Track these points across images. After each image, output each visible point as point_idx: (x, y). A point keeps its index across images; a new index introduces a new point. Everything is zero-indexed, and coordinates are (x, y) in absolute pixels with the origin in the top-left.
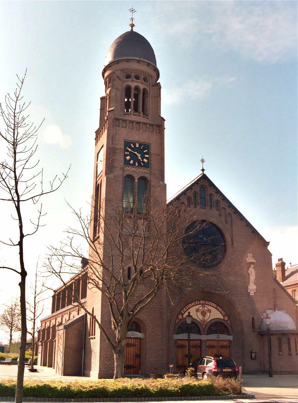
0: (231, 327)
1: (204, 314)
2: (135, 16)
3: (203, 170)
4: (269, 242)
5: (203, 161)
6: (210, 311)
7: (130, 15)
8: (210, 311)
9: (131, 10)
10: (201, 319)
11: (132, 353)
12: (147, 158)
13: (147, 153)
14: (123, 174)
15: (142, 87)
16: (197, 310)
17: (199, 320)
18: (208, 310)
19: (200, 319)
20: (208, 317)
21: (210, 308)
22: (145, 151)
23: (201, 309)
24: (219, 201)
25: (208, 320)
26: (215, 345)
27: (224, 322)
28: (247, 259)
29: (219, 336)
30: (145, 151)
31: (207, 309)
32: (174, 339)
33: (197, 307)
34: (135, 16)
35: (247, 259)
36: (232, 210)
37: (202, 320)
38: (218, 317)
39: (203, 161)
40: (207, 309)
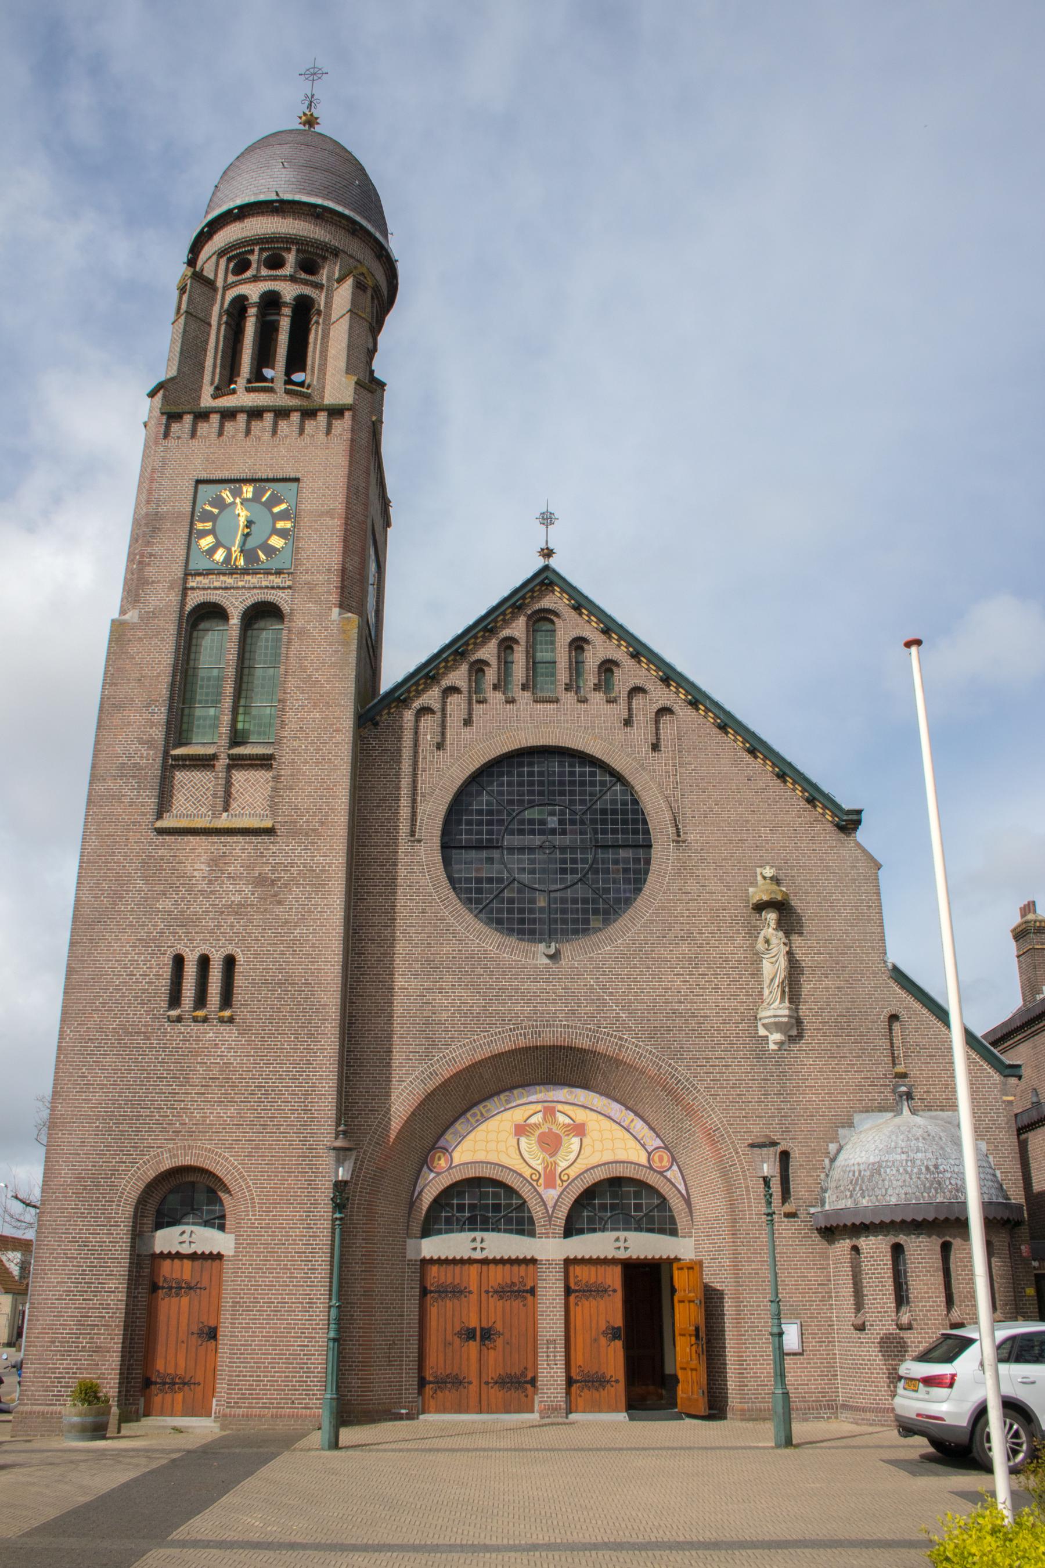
0: (688, 1201)
1: (551, 1143)
2: (320, 90)
3: (548, 553)
4: (859, 812)
5: (547, 519)
6: (579, 1130)
7: (305, 87)
8: (579, 1130)
9: (308, 72)
10: (540, 1168)
11: (184, 1321)
12: (283, 533)
13: (284, 516)
14: (183, 604)
15: (289, 292)
16: (521, 1130)
17: (527, 1172)
18: (569, 1125)
19: (533, 1163)
20: (573, 1156)
21: (580, 1115)
22: (276, 510)
23: (537, 1126)
24: (616, 664)
25: (573, 1172)
26: (609, 1282)
27: (652, 1179)
28: (751, 890)
29: (475, 1249)
30: (276, 510)
31: (568, 1121)
32: (408, 1257)
33: (518, 1115)
34: (320, 90)
35: (751, 890)
36: (677, 693)
37: (545, 1168)
38: (622, 1156)
39: (547, 519)
40: (568, 1121)
